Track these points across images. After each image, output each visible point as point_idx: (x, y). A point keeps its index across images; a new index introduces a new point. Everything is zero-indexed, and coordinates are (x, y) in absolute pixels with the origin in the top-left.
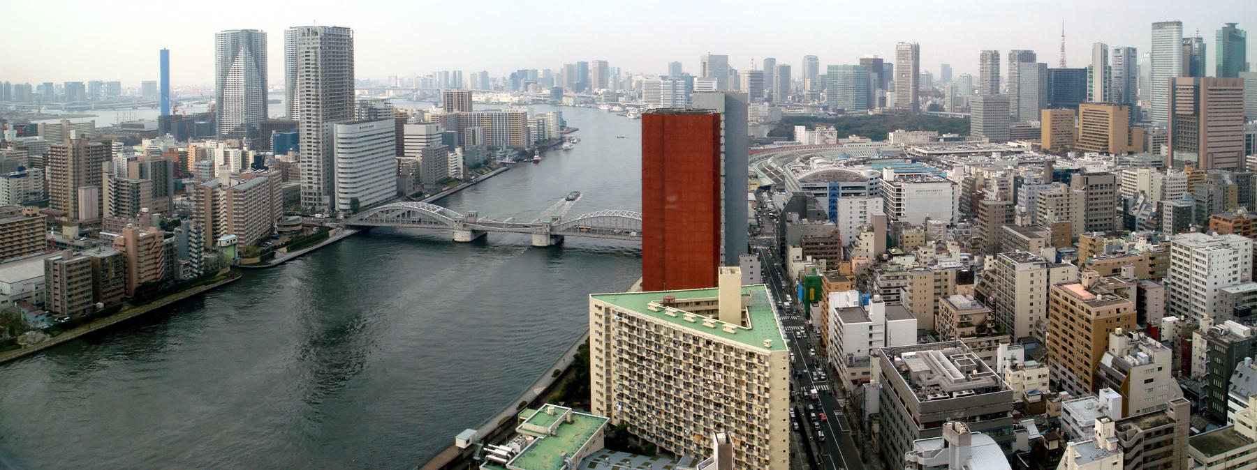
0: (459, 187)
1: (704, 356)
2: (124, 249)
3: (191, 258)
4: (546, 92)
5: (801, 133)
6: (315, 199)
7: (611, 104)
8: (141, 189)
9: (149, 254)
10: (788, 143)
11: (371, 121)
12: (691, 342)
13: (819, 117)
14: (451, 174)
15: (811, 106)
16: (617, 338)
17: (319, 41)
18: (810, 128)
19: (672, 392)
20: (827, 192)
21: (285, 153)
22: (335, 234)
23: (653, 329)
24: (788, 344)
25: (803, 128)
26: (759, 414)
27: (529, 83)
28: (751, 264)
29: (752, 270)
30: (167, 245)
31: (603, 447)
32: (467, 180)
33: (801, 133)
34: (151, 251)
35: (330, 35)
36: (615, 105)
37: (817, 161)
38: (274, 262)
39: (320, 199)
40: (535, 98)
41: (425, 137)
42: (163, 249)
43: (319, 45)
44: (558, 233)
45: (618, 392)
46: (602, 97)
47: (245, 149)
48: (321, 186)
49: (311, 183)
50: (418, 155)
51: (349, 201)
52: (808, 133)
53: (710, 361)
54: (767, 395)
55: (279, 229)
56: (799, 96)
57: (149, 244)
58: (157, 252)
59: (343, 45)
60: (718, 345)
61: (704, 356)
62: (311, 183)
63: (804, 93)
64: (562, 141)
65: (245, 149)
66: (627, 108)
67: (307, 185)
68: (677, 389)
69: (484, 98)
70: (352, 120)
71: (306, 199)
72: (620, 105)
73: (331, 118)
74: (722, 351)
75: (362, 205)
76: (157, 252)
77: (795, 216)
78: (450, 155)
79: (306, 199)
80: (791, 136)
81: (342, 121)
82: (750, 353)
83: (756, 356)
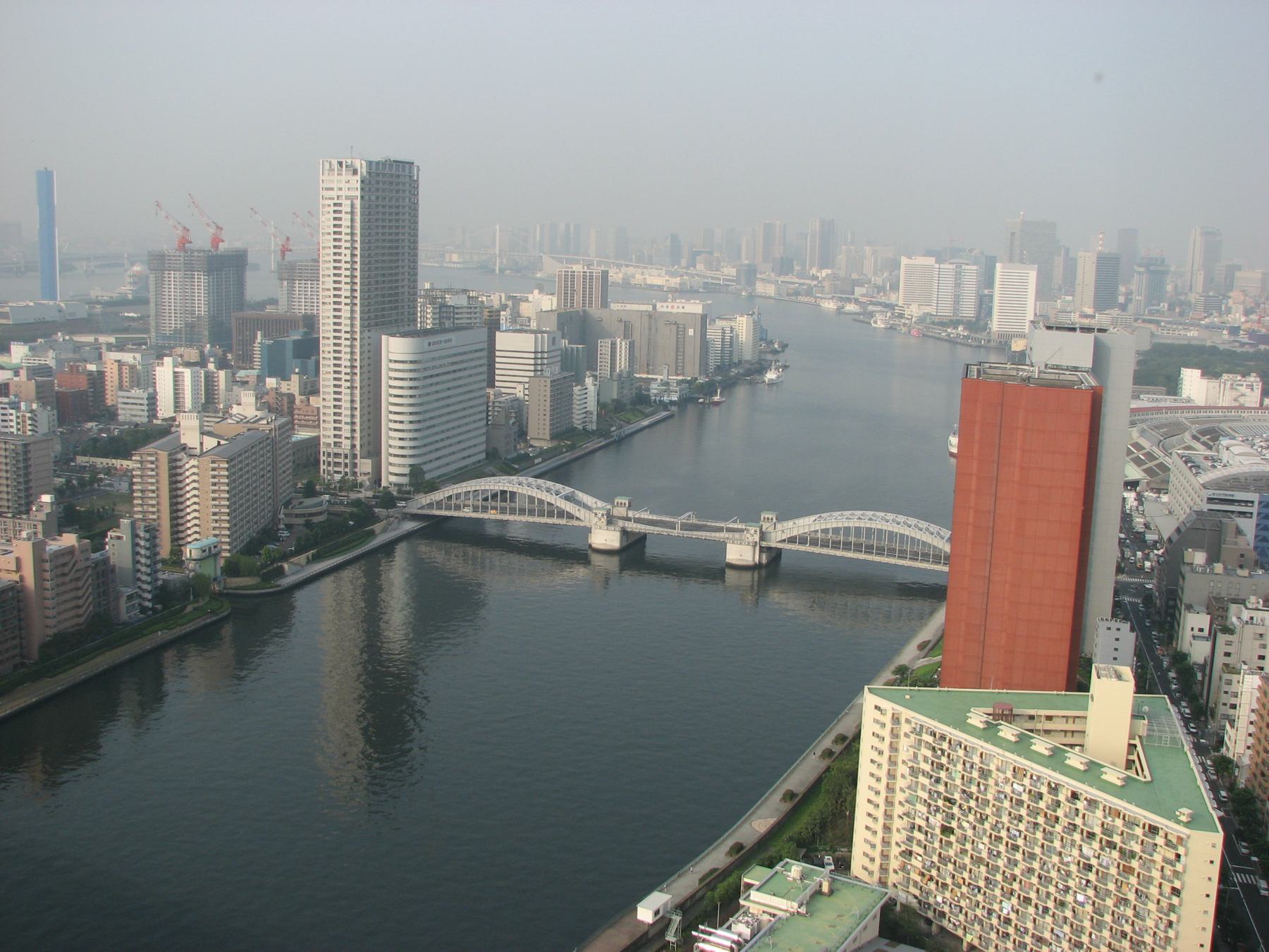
0: (591, 446)
1: (1066, 816)
2: (16, 577)
3: (139, 584)
4: (730, 271)
5: (1193, 384)
6: (346, 465)
7: (841, 299)
8: (31, 462)
9: (64, 584)
10: (1168, 401)
11: (445, 331)
12: (1044, 790)
13: (1221, 347)
14: (577, 422)
15: (1207, 327)
16: (910, 764)
17: (359, 185)
18: (1210, 372)
19: (1000, 863)
20: (1254, 510)
21: (284, 377)
22: (384, 530)
23: (976, 759)
24: (1220, 819)
25: (1197, 372)
26: (1157, 926)
27: (699, 253)
28: (1118, 634)
29: (1117, 645)
30: (97, 564)
31: (877, 933)
32: (601, 433)
33: (1193, 384)
34: (67, 579)
35: (378, 175)
36: (849, 300)
37: (1235, 450)
38: (286, 582)
39: (355, 465)
40: (710, 280)
41: (532, 356)
42: (90, 571)
43: (358, 193)
44: (773, 545)
45: (903, 847)
46: (826, 284)
47: (211, 367)
48: (358, 443)
49: (340, 437)
50: (520, 387)
51: (406, 471)
52: (1205, 382)
53: (1075, 825)
54: (1175, 900)
55: (287, 521)
56: (1181, 304)
57: (64, 565)
58: (78, 579)
59: (401, 187)
60: (1092, 803)
61: (1066, 816)
62: (340, 437)
63: (1192, 297)
64: (761, 369)
65: (211, 367)
66: (871, 308)
67: (332, 440)
68: (1009, 859)
69: (621, 275)
70: (411, 328)
71: (329, 464)
72: (856, 301)
73: (377, 324)
74: (1099, 813)
75: (428, 477)
76: (78, 579)
77: (1199, 558)
78: (576, 389)
79: (329, 455)
80: (1173, 386)
81: (395, 330)
82: (1150, 826)
83: (1161, 833)
